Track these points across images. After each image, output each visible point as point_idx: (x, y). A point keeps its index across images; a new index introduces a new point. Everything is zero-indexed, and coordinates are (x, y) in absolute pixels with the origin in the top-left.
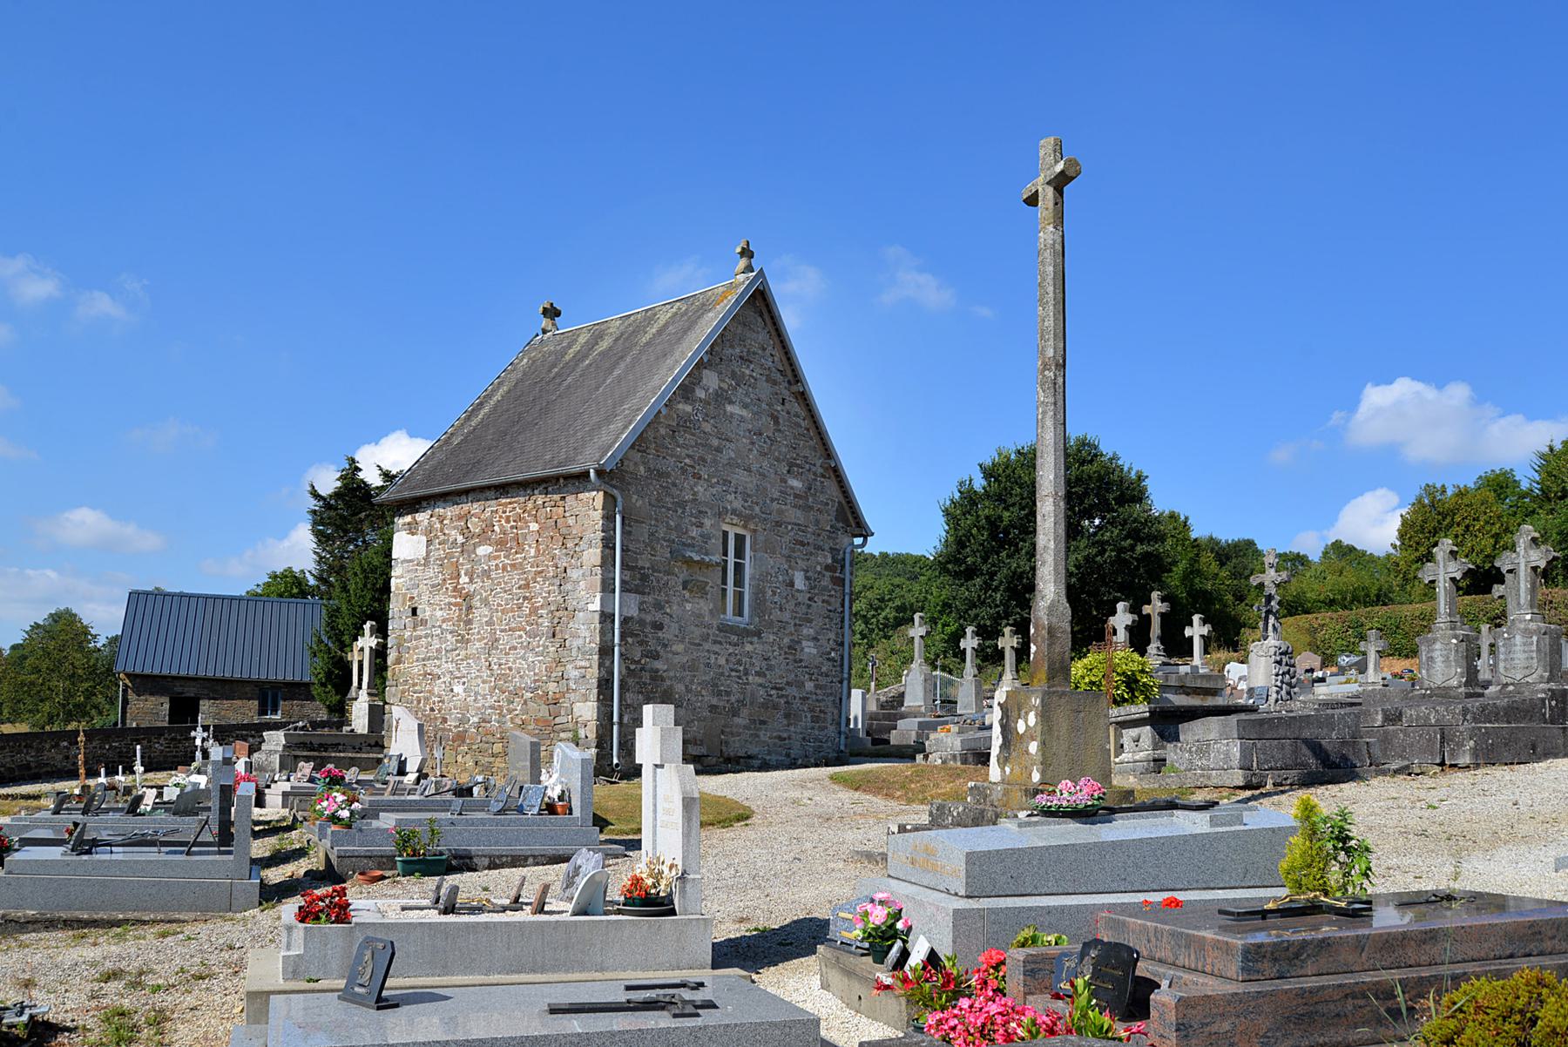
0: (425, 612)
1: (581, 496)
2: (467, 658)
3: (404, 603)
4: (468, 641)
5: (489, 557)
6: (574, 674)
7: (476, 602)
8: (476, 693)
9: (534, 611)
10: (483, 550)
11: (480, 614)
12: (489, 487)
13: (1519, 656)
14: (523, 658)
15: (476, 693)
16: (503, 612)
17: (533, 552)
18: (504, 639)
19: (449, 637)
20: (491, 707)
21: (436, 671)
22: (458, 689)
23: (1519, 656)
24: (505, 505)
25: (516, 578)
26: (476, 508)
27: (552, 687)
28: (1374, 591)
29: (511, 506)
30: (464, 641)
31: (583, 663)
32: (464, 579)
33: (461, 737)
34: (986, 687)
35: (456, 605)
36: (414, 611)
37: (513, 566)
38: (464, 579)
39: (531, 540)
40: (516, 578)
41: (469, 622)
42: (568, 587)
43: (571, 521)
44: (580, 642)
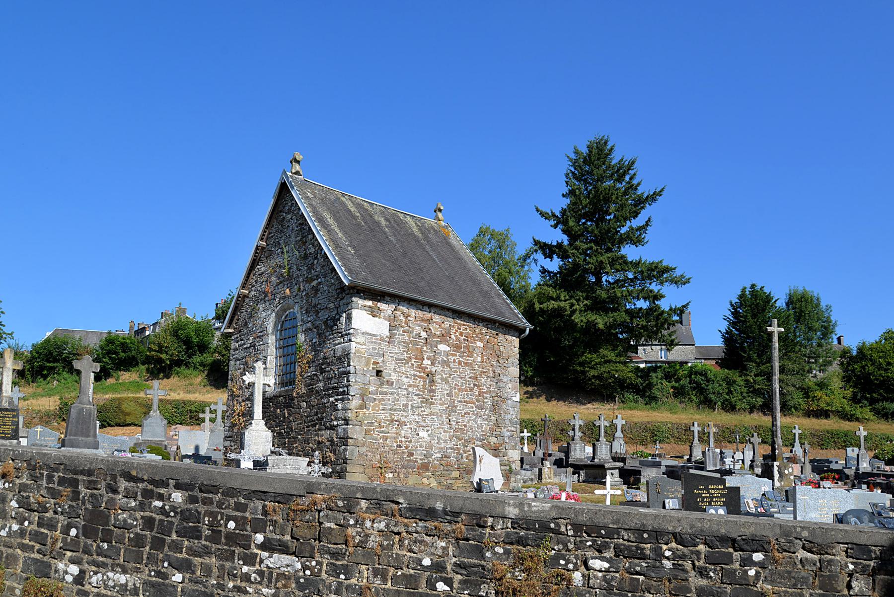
0: (390, 373)
1: (507, 337)
2: (431, 414)
3: (367, 364)
4: (432, 403)
5: (447, 354)
6: (507, 434)
7: (437, 378)
8: (439, 439)
9: (481, 394)
10: (443, 347)
11: (441, 389)
12: (449, 309)
13: (604, 451)
14: (475, 420)
15: (439, 439)
16: (459, 390)
17: (479, 359)
18: (460, 407)
19: (416, 398)
20: (451, 448)
21: (403, 419)
22: (423, 434)
23: (604, 451)
24: (460, 324)
25: (468, 372)
26: (437, 318)
27: (493, 440)
28: (418, 457)
29: (465, 327)
30: (428, 402)
31: (512, 429)
32: (427, 362)
33: (425, 467)
34: (172, 433)
35: (420, 377)
36: (379, 373)
37: (466, 363)
38: (427, 362)
39: (477, 351)
40: (468, 372)
41: (433, 391)
42: (501, 384)
43: (502, 349)
44: (510, 417)
